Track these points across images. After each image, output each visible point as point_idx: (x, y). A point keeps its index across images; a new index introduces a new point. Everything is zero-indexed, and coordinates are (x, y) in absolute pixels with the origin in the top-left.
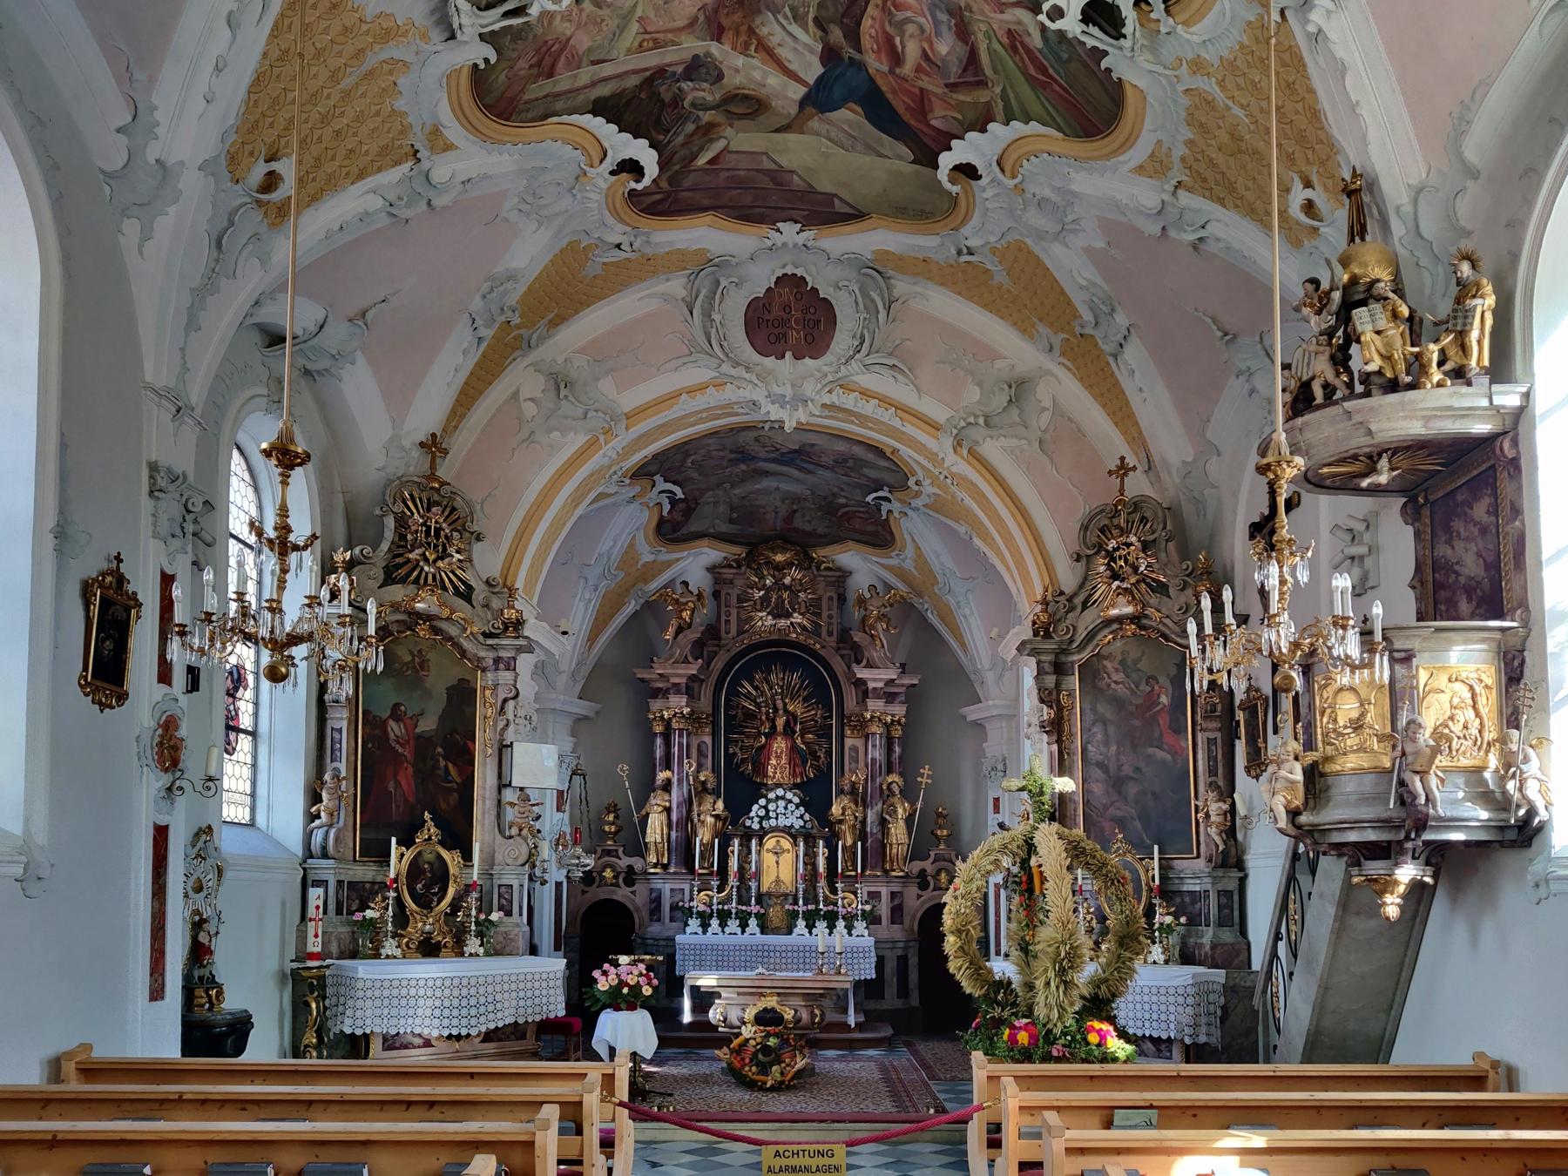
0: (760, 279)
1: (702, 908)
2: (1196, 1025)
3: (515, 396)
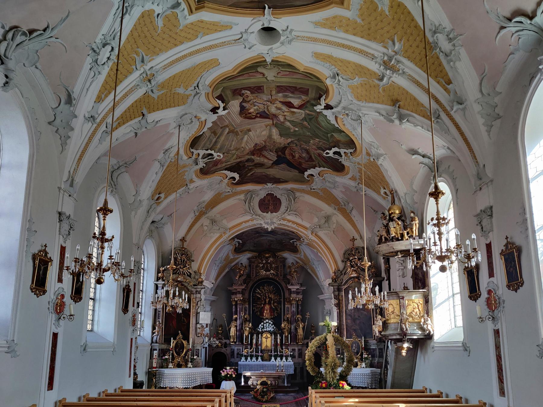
0: (262, 194)
1: (245, 354)
2: (372, 383)
3: (202, 225)
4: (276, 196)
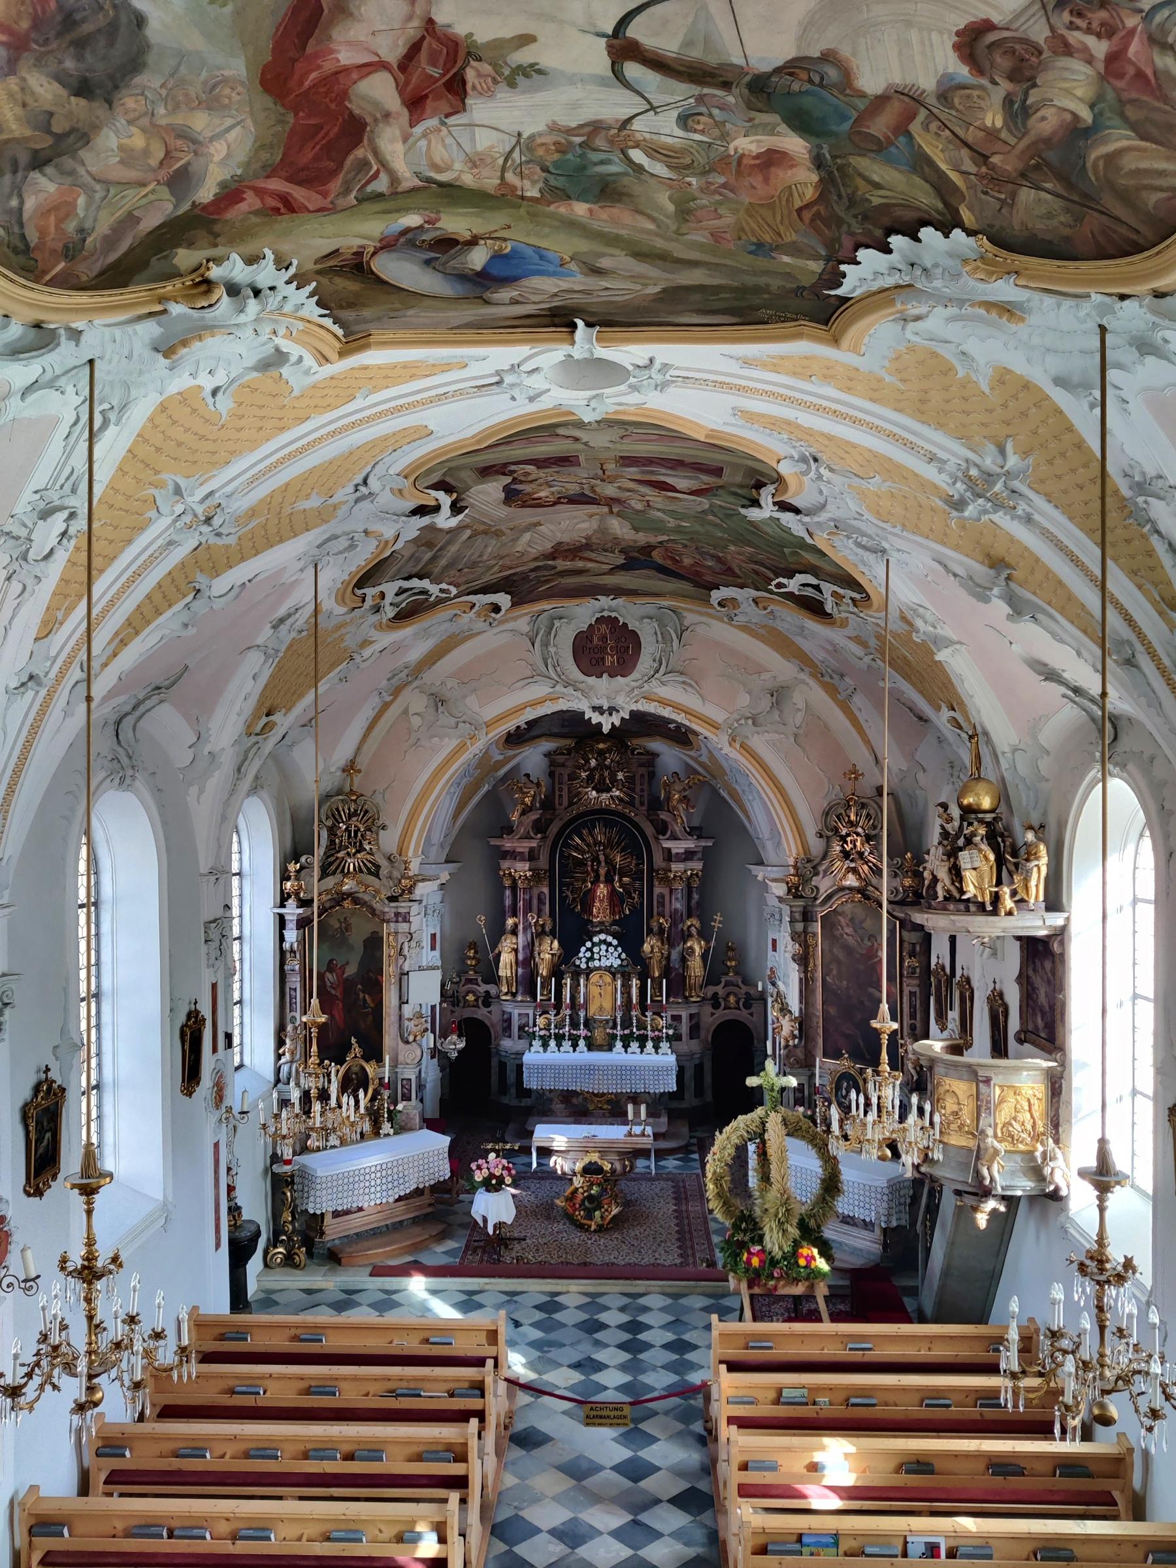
1: (542, 1033)
2: (889, 1215)
3: (406, 712)
4: (625, 625)
